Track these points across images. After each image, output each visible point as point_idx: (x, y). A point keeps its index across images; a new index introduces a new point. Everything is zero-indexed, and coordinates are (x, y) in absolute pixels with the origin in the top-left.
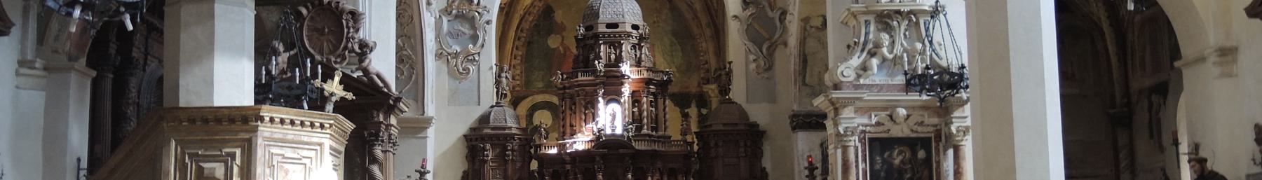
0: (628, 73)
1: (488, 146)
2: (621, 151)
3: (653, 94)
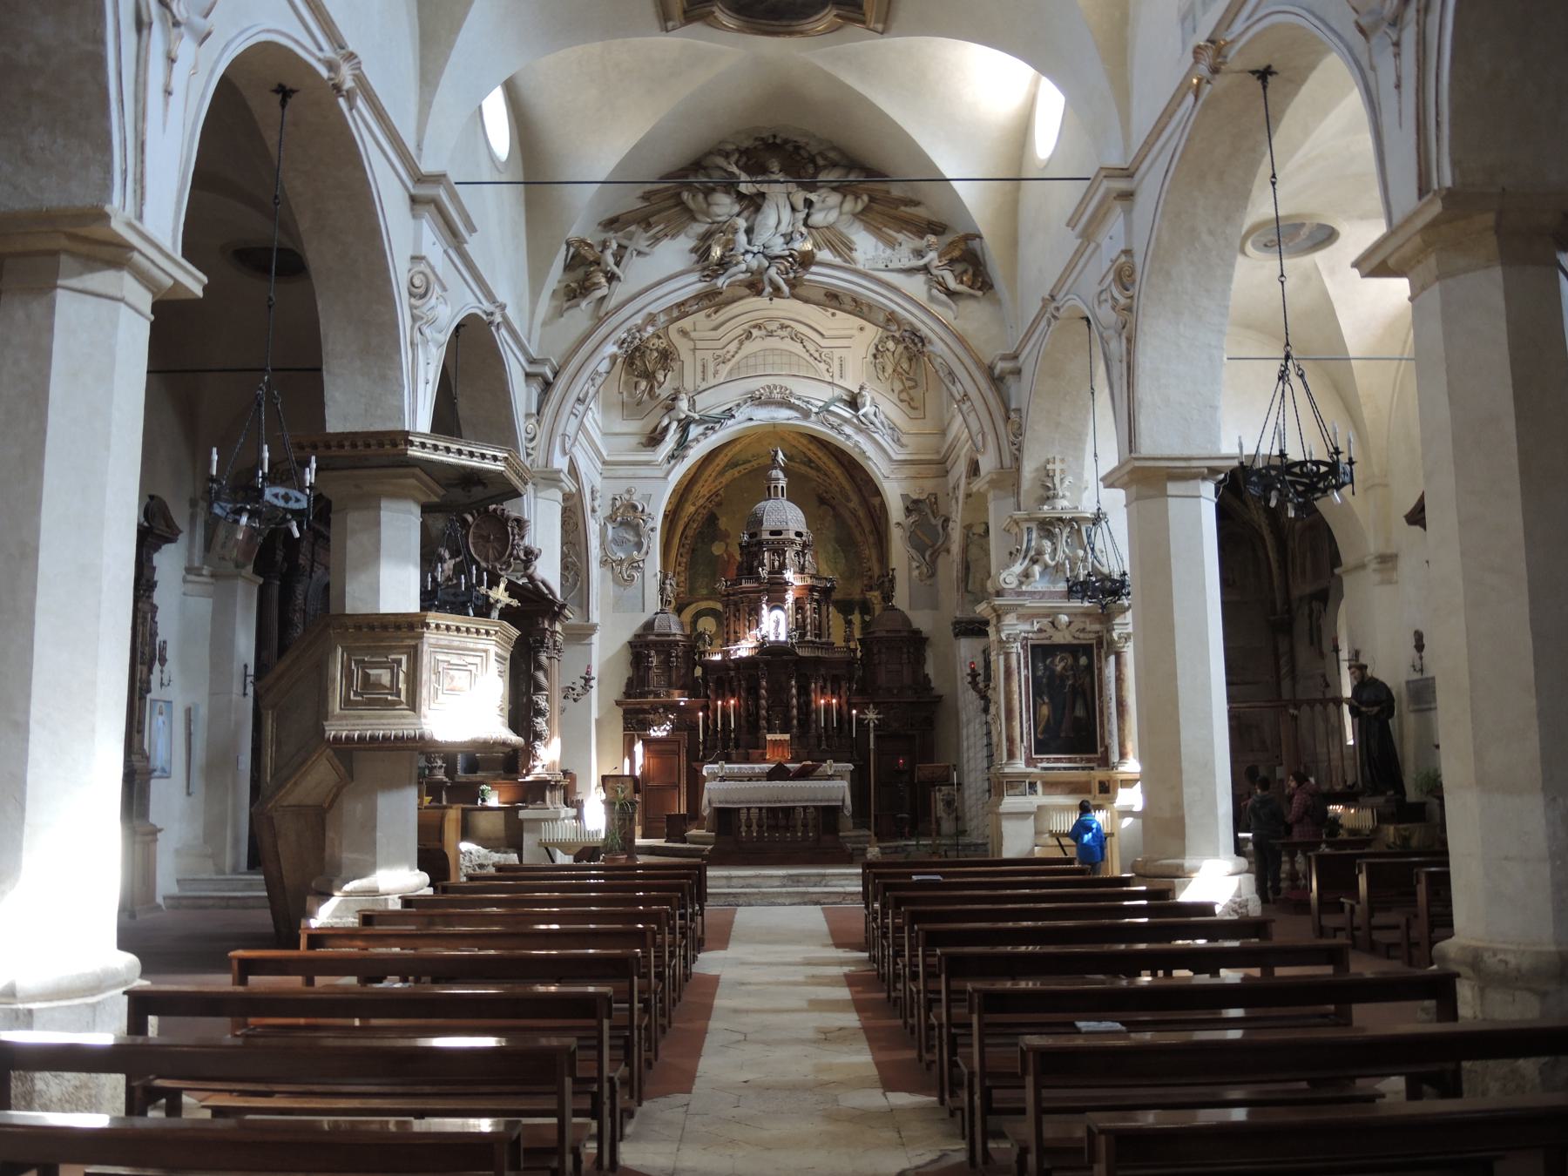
1: (653, 653)
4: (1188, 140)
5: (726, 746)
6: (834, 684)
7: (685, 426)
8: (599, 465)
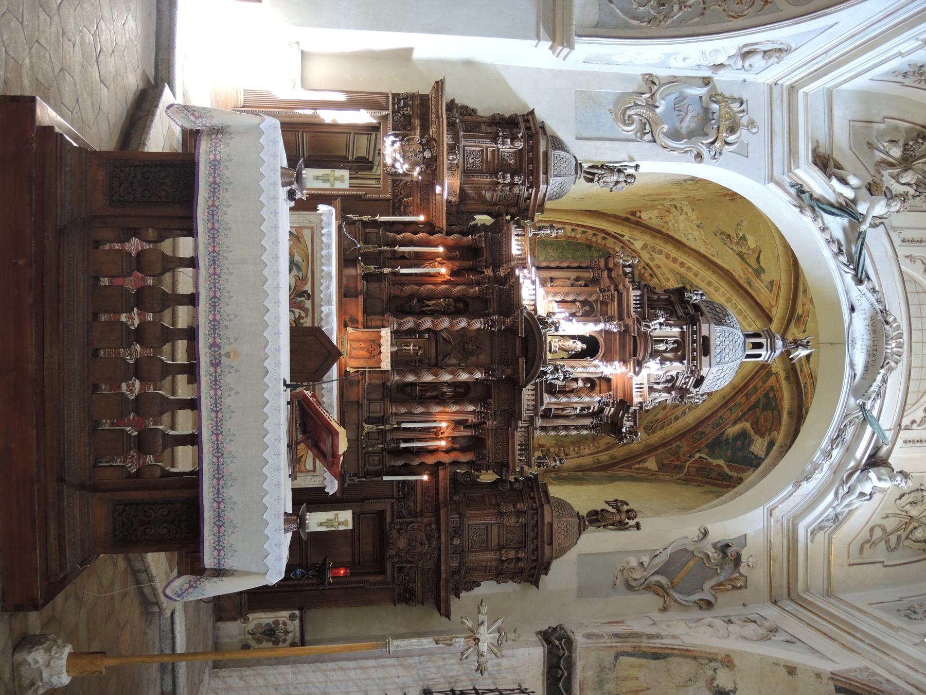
0: (644, 372)
1: (519, 145)
2: (522, 361)
3: (601, 410)
4: (508, 454)
5: (367, 258)
6: (472, 443)
7: (845, 208)
8: (787, 82)
